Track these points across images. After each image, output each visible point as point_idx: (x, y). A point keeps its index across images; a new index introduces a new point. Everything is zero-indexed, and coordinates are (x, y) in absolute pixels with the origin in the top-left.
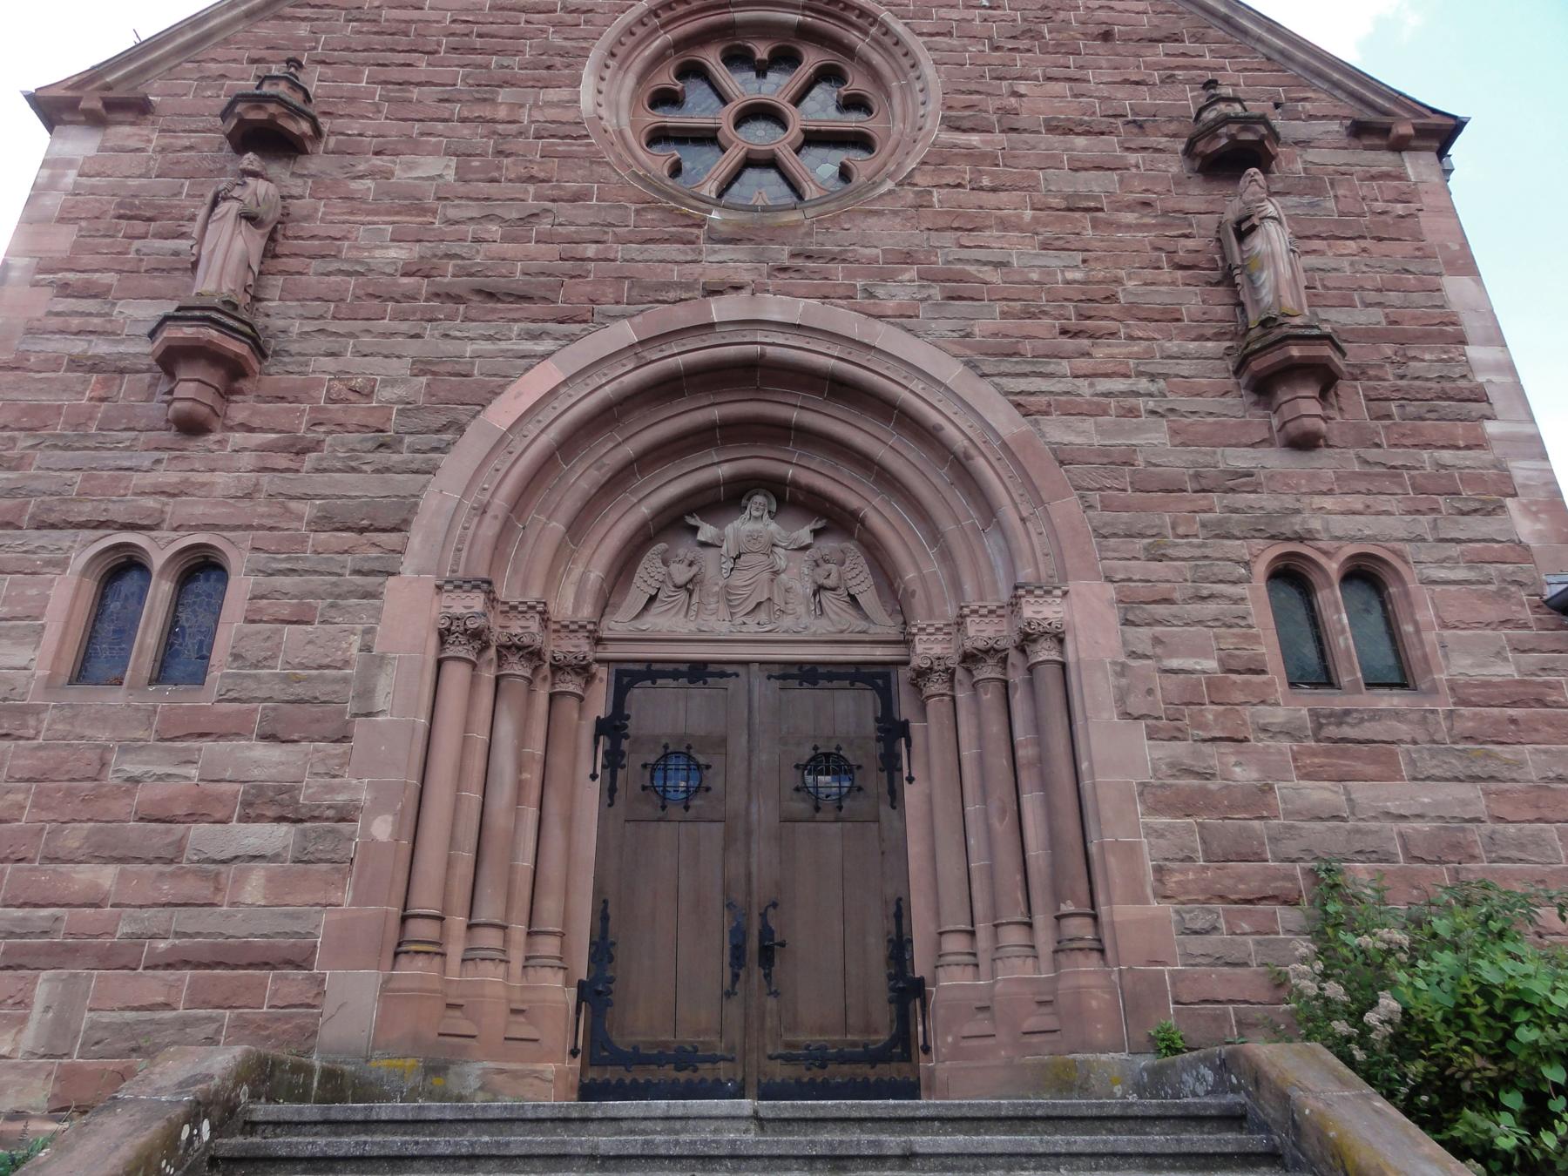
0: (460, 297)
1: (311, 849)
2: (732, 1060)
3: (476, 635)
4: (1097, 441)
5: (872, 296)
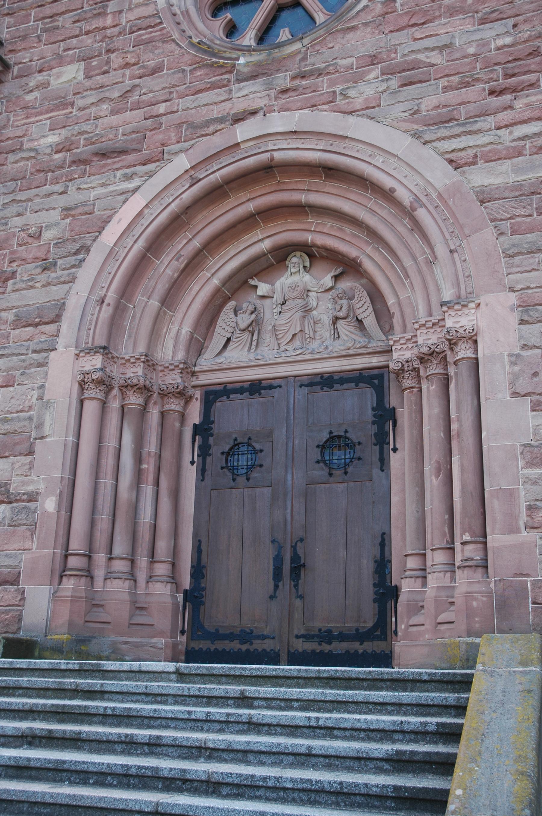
0: (86, 160)
1: (15, 519)
2: (274, 638)
3: (100, 382)
4: (513, 178)
5: (346, 96)
